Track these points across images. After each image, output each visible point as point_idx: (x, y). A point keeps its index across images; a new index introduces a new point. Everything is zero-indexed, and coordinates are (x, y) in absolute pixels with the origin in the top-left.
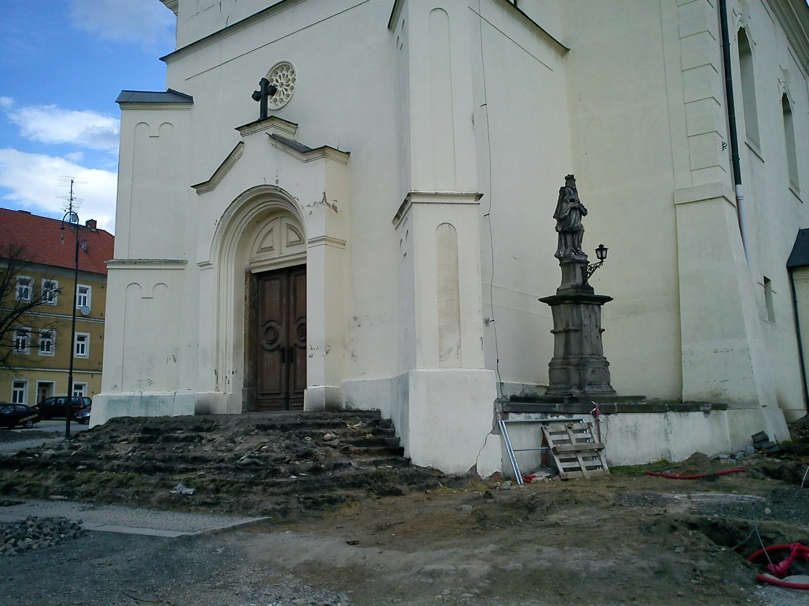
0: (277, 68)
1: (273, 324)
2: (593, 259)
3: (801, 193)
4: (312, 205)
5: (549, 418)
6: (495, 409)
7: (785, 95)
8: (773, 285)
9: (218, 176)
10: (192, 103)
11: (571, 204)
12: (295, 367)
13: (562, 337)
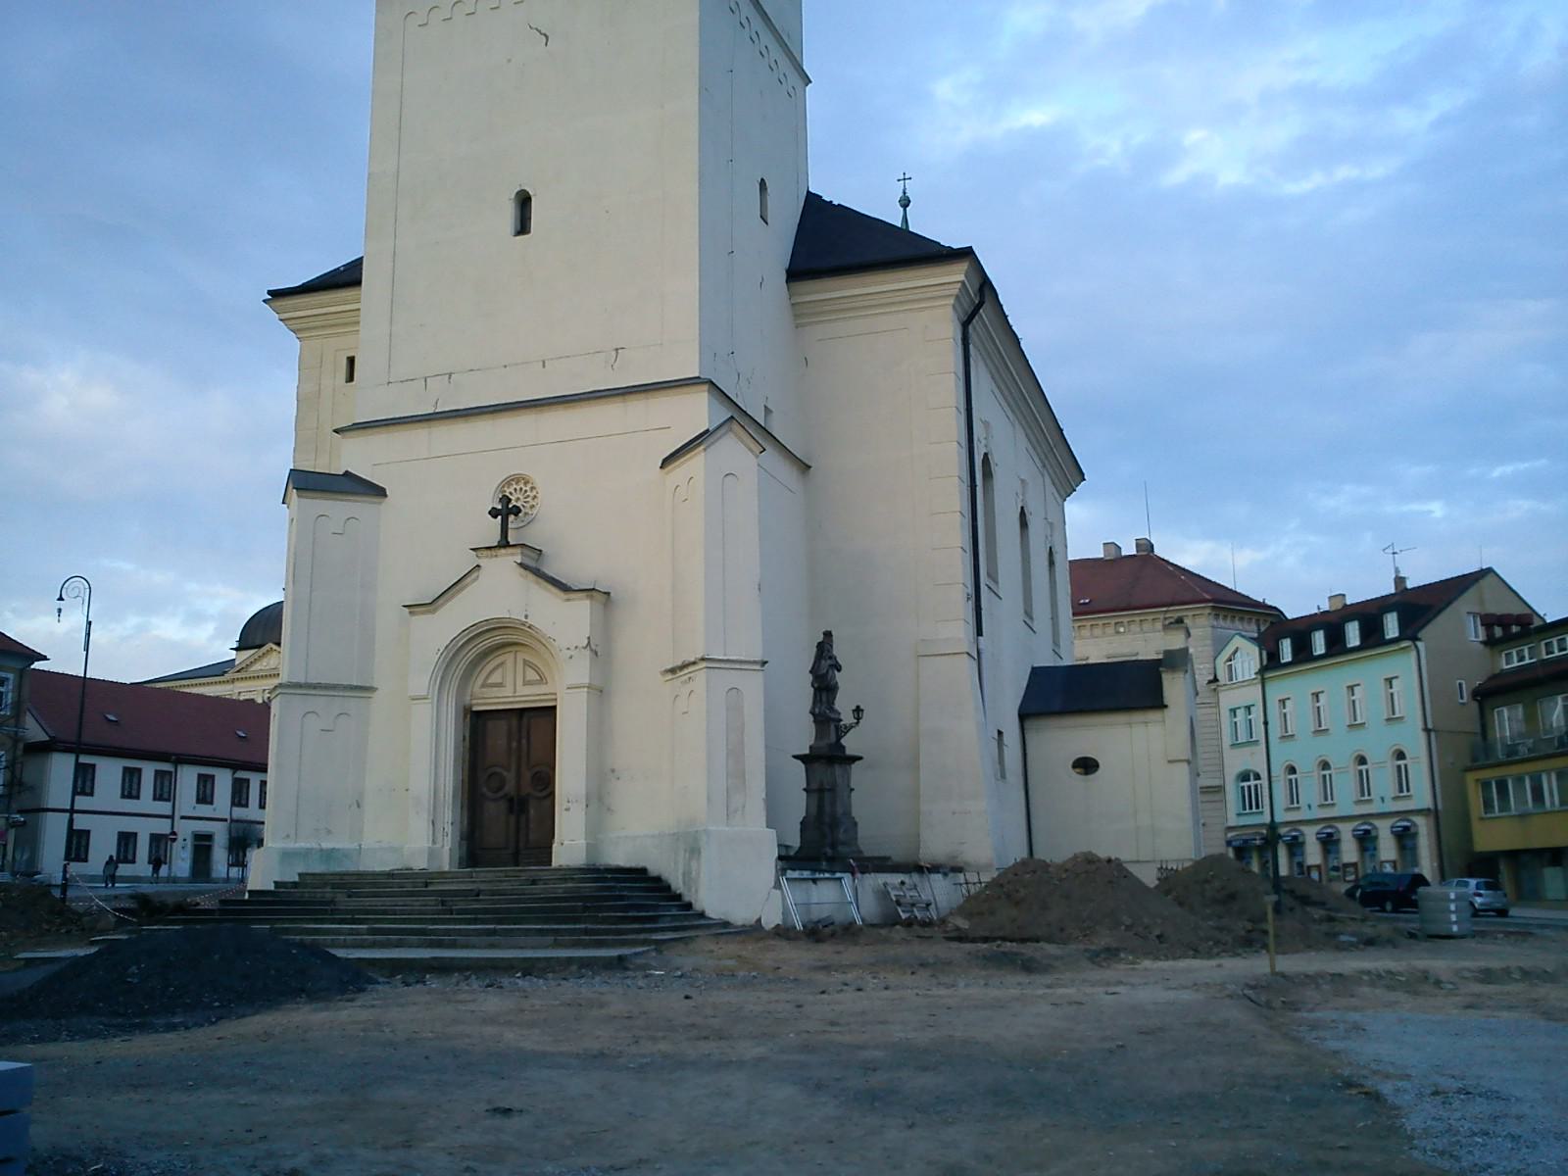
0: (513, 480)
1: (498, 770)
2: (847, 718)
3: (1035, 622)
4: (573, 648)
5: (817, 876)
6: (776, 866)
7: (1022, 508)
8: (1006, 738)
9: (446, 596)
10: (385, 495)
11: (829, 662)
12: (528, 820)
13: (815, 797)
